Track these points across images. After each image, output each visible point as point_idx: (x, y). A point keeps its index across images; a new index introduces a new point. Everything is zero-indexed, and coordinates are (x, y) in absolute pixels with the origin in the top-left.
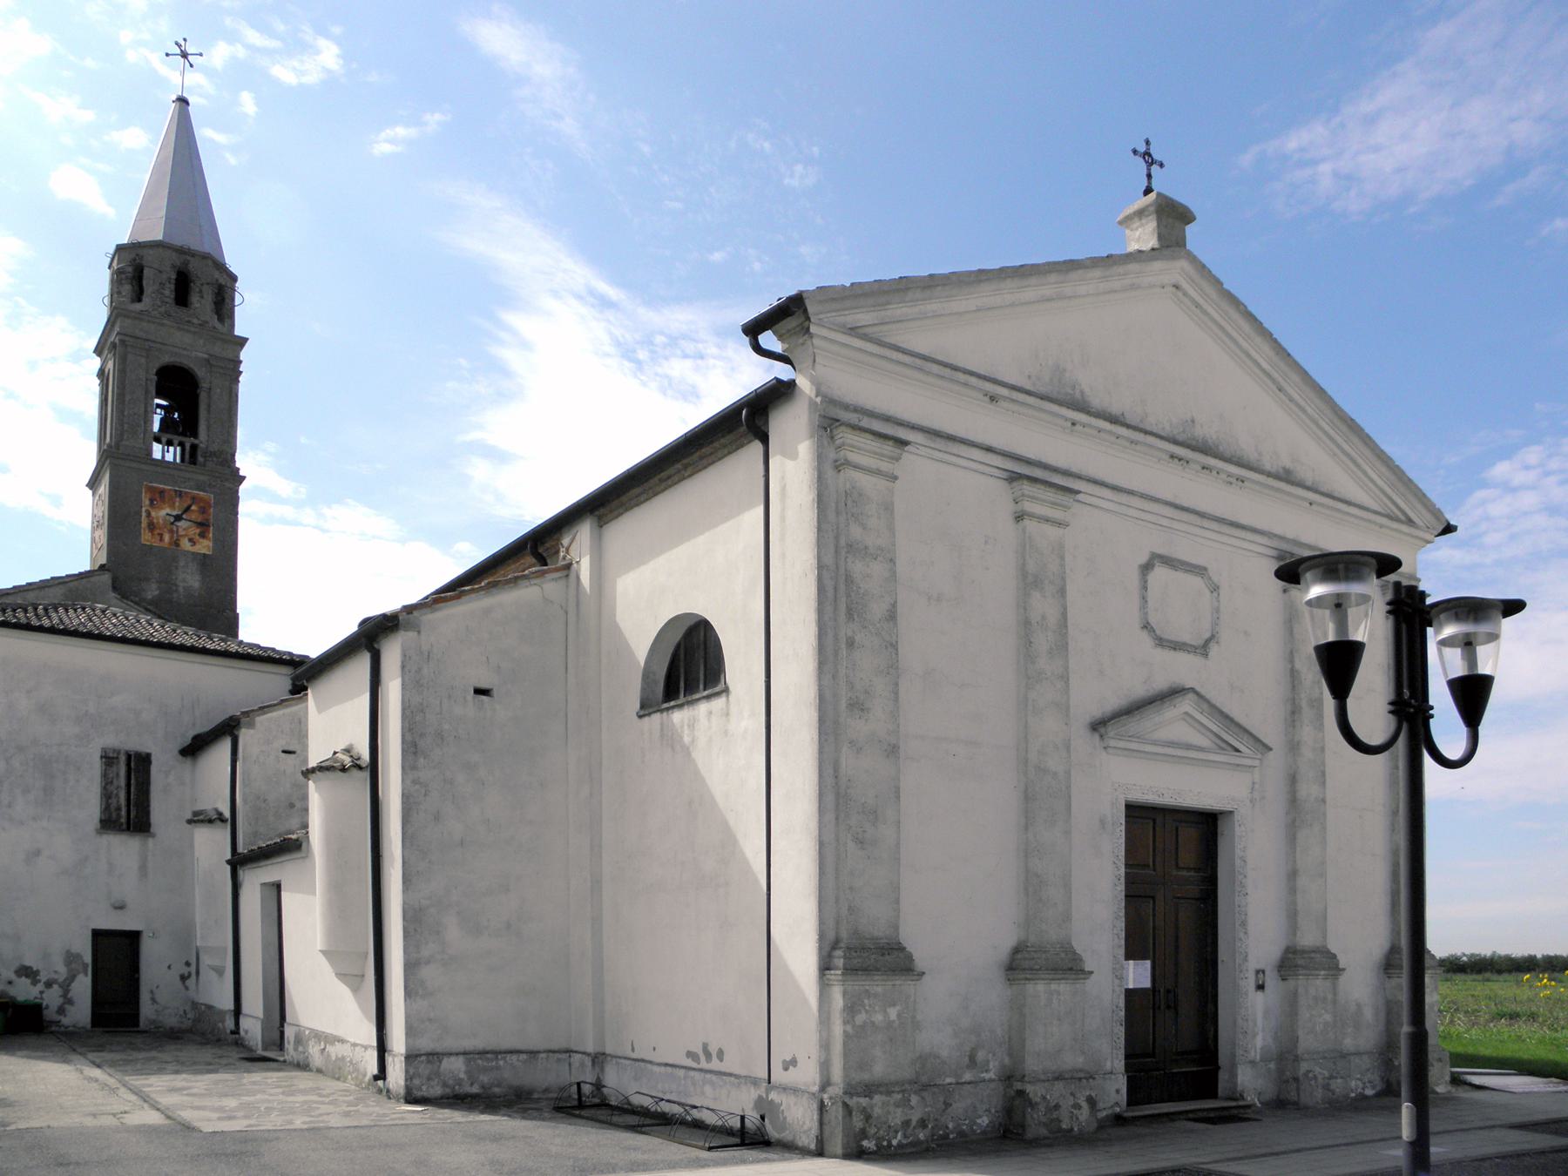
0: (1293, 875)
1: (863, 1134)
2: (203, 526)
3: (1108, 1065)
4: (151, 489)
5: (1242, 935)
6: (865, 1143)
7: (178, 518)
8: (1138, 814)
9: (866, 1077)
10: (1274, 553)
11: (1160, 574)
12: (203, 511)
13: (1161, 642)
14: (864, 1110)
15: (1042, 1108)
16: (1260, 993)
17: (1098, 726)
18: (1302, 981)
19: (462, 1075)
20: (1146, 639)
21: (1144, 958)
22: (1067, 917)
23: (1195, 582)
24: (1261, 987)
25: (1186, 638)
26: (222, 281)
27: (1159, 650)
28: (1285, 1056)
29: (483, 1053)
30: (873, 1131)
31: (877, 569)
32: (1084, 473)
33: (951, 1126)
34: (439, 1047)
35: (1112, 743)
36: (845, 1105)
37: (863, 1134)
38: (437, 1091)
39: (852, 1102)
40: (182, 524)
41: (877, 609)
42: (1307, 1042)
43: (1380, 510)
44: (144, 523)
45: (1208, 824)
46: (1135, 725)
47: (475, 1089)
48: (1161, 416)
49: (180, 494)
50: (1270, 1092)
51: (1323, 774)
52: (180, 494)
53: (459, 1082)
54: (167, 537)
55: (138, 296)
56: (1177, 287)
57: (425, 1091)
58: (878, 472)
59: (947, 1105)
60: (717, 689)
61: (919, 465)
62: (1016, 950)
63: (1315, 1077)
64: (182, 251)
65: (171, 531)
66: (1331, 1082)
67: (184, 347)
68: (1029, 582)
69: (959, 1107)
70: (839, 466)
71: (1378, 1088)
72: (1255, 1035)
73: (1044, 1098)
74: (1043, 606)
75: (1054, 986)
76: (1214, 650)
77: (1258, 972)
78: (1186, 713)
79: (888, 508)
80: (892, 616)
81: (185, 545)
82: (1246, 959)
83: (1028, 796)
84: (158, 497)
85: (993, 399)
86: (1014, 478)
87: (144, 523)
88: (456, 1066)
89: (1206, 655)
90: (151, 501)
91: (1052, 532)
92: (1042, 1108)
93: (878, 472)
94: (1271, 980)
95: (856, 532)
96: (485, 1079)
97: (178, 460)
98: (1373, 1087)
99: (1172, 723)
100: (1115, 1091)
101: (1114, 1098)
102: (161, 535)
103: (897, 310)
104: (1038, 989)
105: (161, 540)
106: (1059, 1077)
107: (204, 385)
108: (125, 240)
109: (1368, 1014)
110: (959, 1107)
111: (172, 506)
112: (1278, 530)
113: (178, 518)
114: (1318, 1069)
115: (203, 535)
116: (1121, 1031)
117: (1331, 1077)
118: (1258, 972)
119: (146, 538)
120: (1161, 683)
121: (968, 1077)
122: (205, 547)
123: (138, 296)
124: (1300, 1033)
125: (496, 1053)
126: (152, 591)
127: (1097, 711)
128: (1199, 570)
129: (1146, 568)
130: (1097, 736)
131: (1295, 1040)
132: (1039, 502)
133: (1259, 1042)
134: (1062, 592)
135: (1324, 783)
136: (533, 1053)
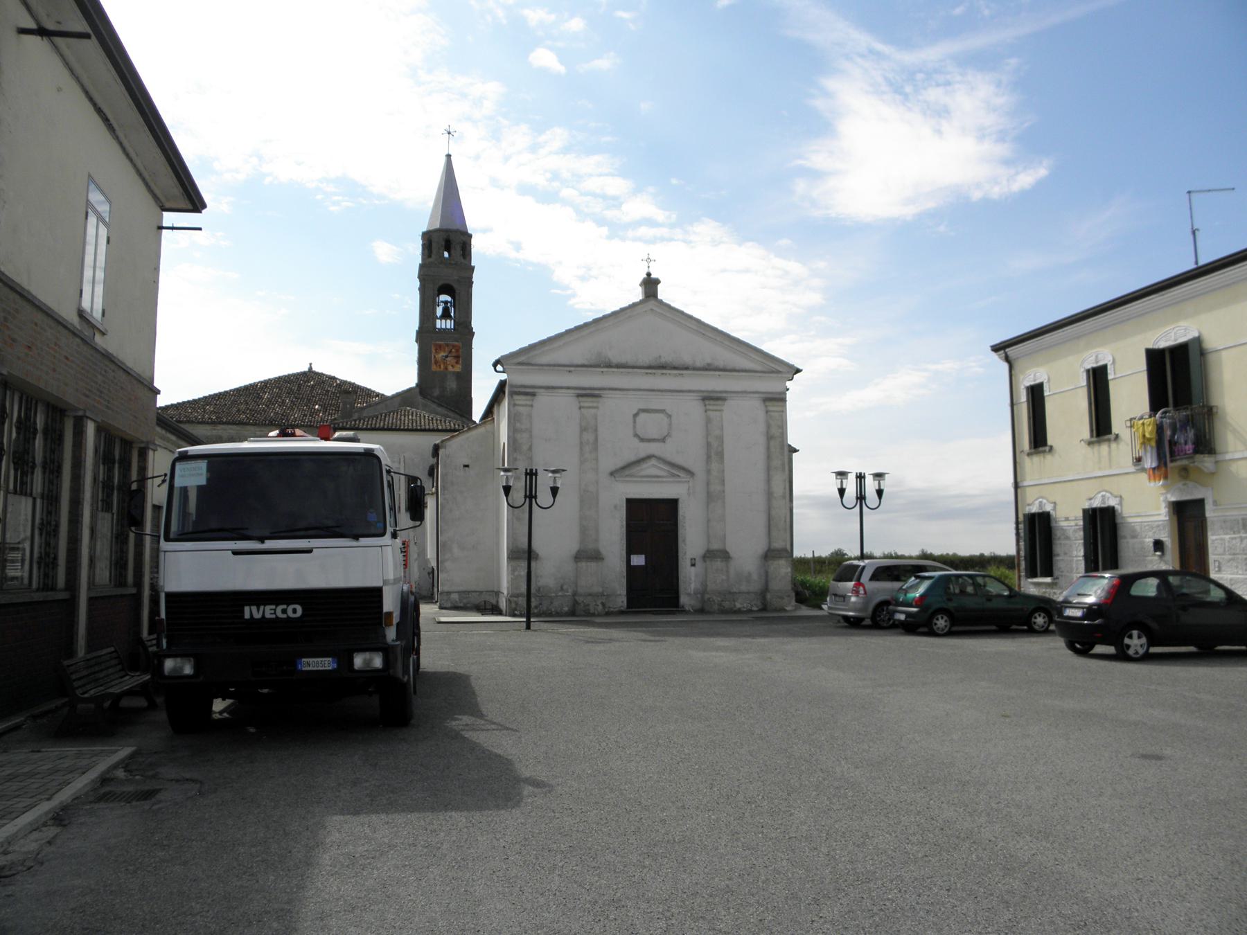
0: (708, 521)
1: (516, 609)
2: (457, 357)
3: (619, 593)
4: (436, 345)
5: (683, 545)
6: (516, 612)
7: (447, 357)
8: (630, 502)
9: (518, 592)
10: (700, 398)
11: (642, 416)
12: (457, 351)
13: (642, 440)
14: (515, 602)
15: (582, 605)
16: (693, 568)
17: (612, 474)
18: (770, 562)
19: (457, 600)
20: (636, 440)
21: (641, 554)
22: (597, 540)
23: (661, 416)
24: (693, 565)
25: (656, 437)
26: (464, 239)
27: (641, 443)
28: (702, 592)
29: (464, 592)
30: (518, 609)
31: (525, 435)
32: (605, 387)
33: (553, 610)
34: (450, 590)
35: (617, 479)
36: (509, 600)
37: (516, 609)
38: (449, 605)
39: (511, 599)
40: (449, 359)
41: (525, 448)
42: (711, 586)
43: (764, 369)
44: (433, 361)
45: (671, 505)
46: (634, 470)
47: (461, 605)
48: (645, 359)
49: (447, 345)
50: (698, 605)
51: (724, 481)
52: (447, 345)
53: (456, 602)
54: (442, 366)
55: (430, 256)
56: (652, 310)
57: (445, 605)
58: (526, 405)
59: (552, 603)
60: (718, 408)
61: (543, 400)
62: (578, 551)
63: (714, 601)
64: (447, 231)
65: (444, 363)
66: (723, 603)
67: (450, 276)
68: (583, 429)
69: (556, 603)
70: (515, 405)
71: (760, 607)
72: (690, 583)
73: (583, 602)
74: (589, 436)
75: (589, 564)
76: (668, 440)
77: (691, 559)
78: (653, 465)
79: (530, 416)
80: (530, 449)
81: (450, 368)
82: (685, 554)
83: (582, 501)
84: (439, 348)
85: (570, 371)
86: (579, 396)
87: (433, 361)
88: (455, 597)
89: (664, 442)
90: (436, 350)
91: (593, 411)
92: (582, 605)
93: (526, 405)
94: (699, 563)
95: (518, 425)
96: (465, 601)
97: (452, 327)
98: (757, 607)
99: (649, 469)
100: (621, 601)
101: (621, 604)
102: (440, 366)
103: (531, 354)
104: (583, 565)
105: (440, 367)
106: (590, 595)
107: (457, 291)
108: (425, 229)
109: (755, 577)
110: (556, 603)
111: (445, 352)
112: (703, 389)
113: (447, 357)
114: (715, 598)
115: (457, 363)
116: (624, 581)
117: (722, 601)
118: (691, 559)
119: (434, 368)
120: (642, 454)
121: (560, 594)
122: (458, 368)
123: (430, 256)
124: (708, 583)
125: (469, 592)
126: (436, 392)
127: (613, 468)
128: (662, 411)
129: (636, 415)
130: (613, 478)
131: (707, 585)
132: (587, 402)
133: (693, 586)
134: (596, 430)
135: (724, 485)
136: (481, 592)
